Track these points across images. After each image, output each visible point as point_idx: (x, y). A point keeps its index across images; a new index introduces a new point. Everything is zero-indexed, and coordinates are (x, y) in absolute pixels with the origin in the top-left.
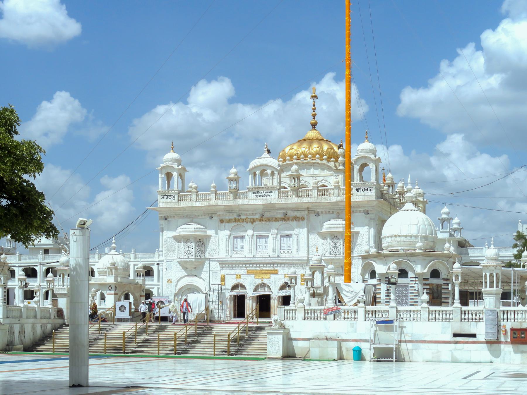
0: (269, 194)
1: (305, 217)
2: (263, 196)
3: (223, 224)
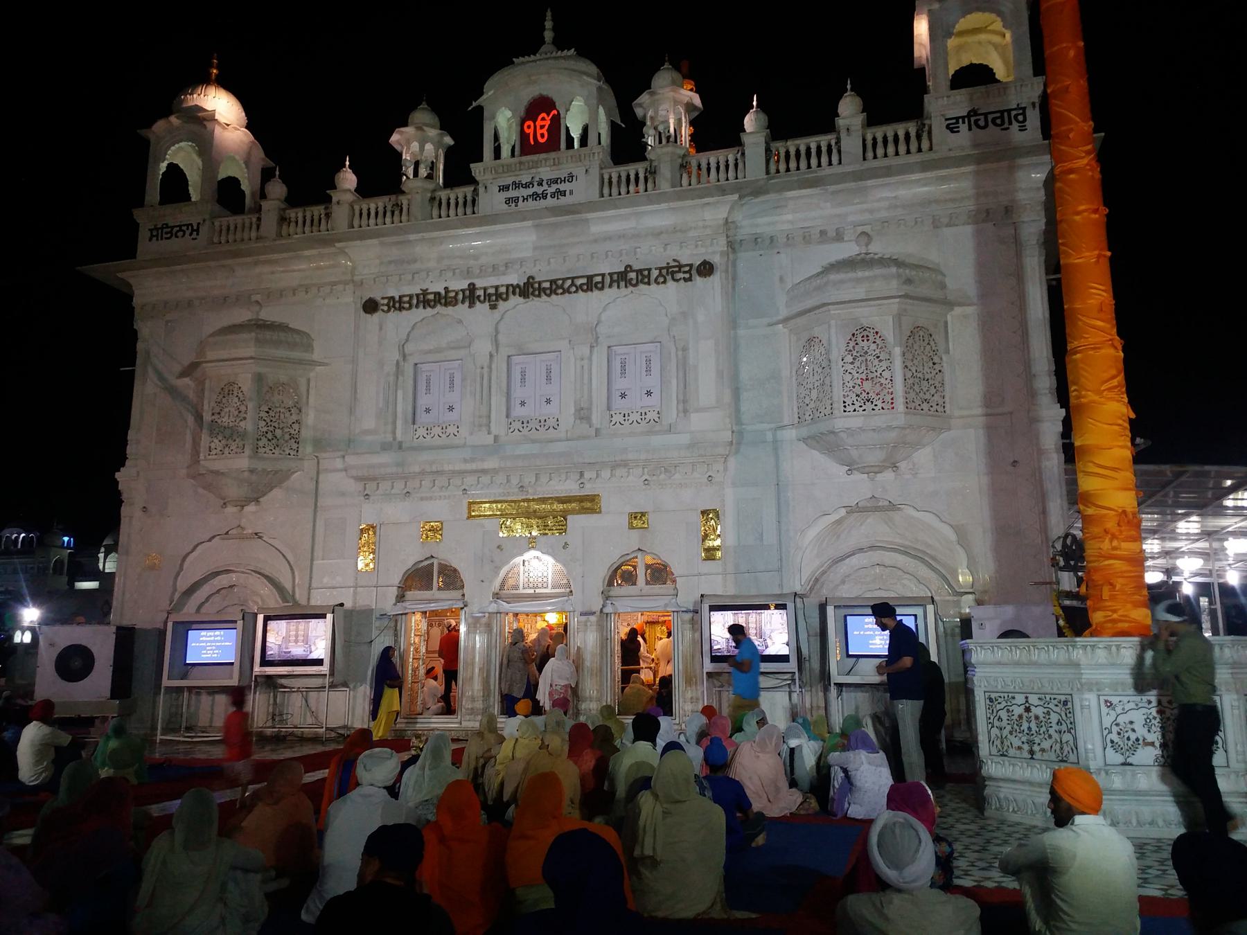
0: (562, 187)
1: (716, 260)
2: (535, 196)
3: (376, 317)
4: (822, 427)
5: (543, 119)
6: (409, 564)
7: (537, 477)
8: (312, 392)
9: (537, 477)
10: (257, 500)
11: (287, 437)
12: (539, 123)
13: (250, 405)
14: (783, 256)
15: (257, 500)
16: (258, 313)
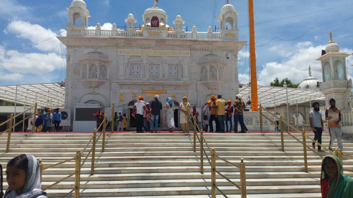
4: (206, 82)
5: (156, 21)
6: (130, 101)
7: (155, 86)
8: (109, 67)
9: (155, 86)
10: (98, 87)
11: (104, 75)
12: (155, 22)
13: (98, 69)
14: (199, 52)
15: (98, 87)
16: (96, 50)
